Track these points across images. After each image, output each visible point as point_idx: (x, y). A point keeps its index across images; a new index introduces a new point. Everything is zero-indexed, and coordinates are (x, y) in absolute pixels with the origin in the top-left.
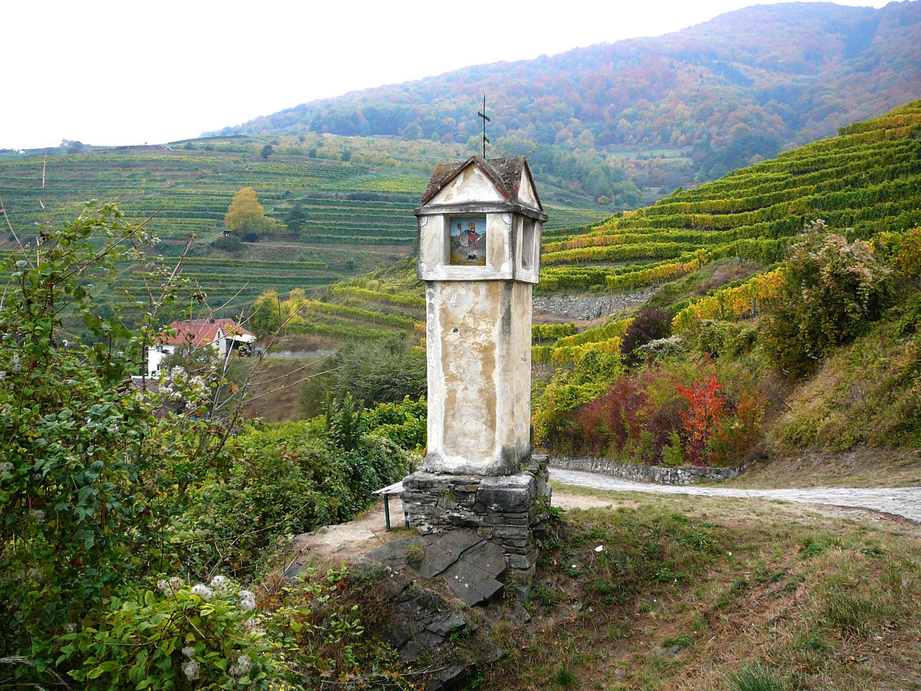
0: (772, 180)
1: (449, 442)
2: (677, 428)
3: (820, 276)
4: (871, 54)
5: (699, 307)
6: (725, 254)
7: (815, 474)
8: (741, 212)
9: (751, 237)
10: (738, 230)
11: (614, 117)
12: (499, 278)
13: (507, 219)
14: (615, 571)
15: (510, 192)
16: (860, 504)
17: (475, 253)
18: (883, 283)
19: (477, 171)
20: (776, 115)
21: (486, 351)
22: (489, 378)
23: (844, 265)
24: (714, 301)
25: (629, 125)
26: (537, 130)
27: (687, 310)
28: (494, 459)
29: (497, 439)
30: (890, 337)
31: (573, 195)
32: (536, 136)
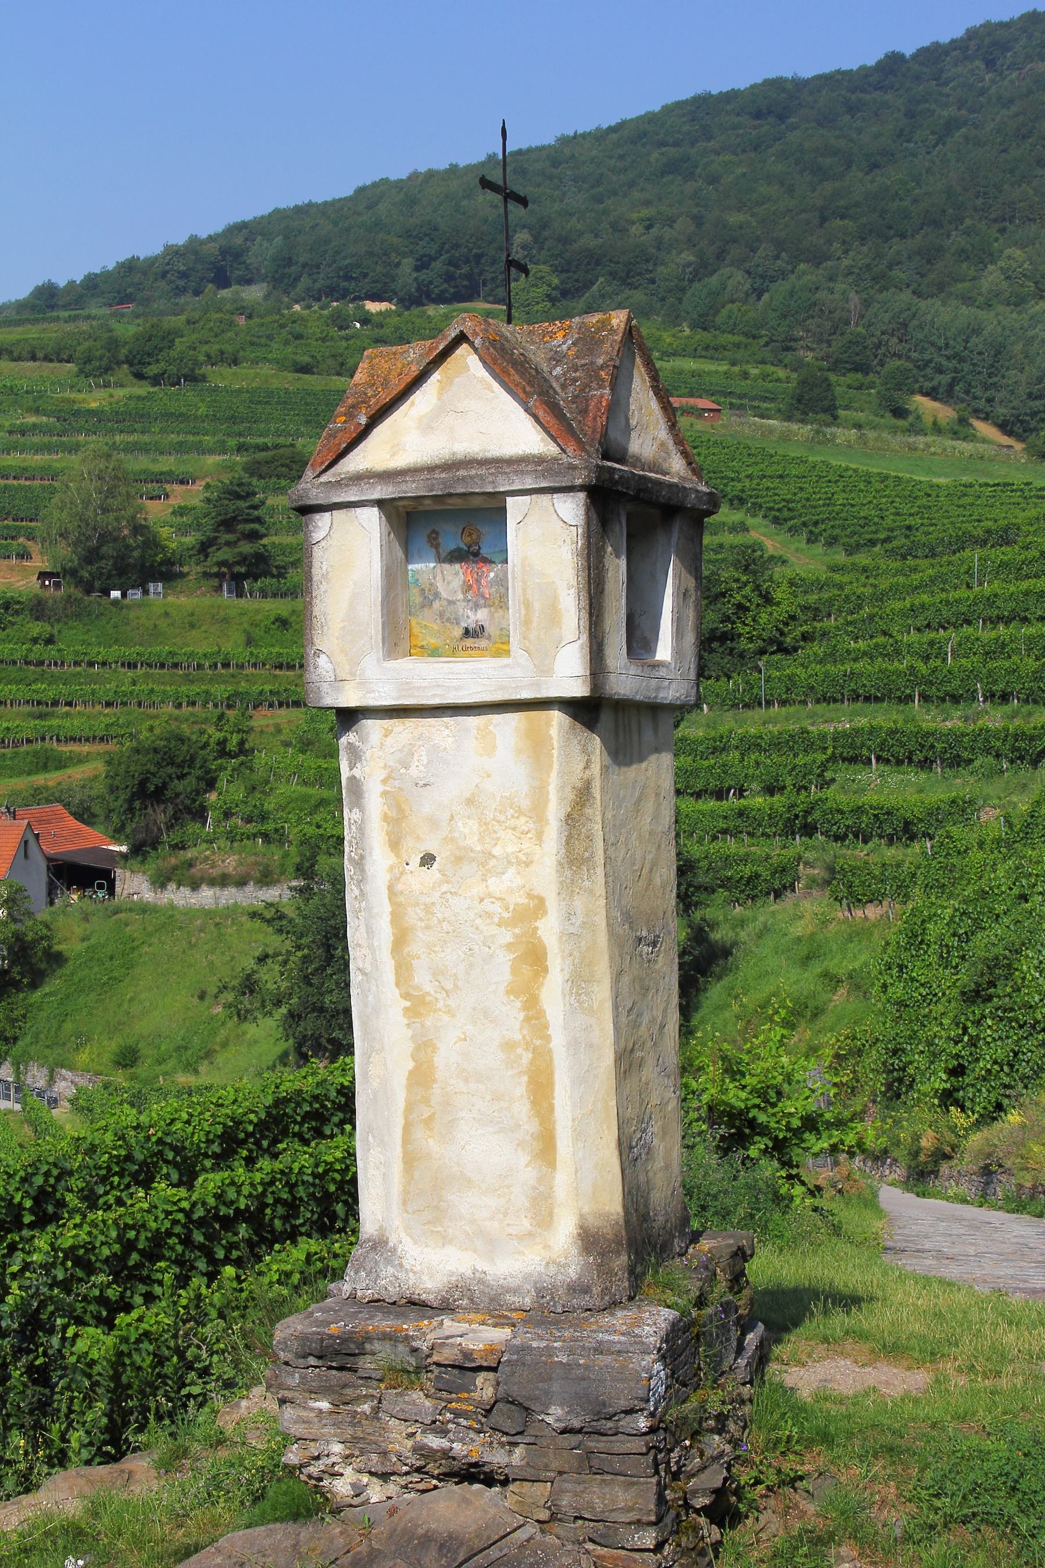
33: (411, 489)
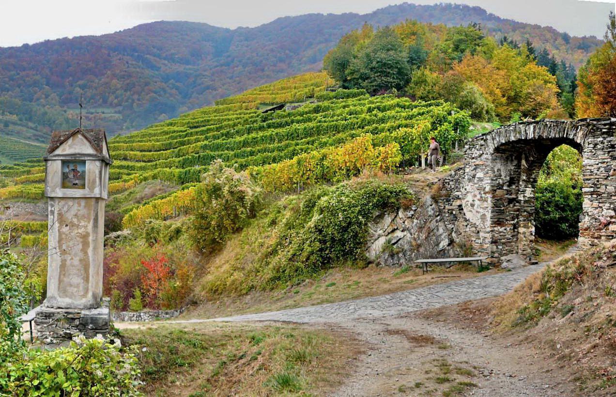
0: (178, 132)
1: (61, 289)
2: (139, 287)
4: (229, 56)
5: (140, 211)
6: (151, 178)
7: (229, 310)
8: (158, 151)
9: (166, 167)
10: (158, 162)
11: (72, 86)
12: (93, 196)
13: (98, 163)
14: (155, 362)
17: (77, 182)
18: (256, 197)
19: (80, 136)
20: (174, 90)
21: (85, 237)
22: (86, 253)
23: (236, 186)
24: (149, 207)
25: (82, 91)
26: (21, 92)
27: (132, 213)
28: (89, 299)
29: (90, 288)
30: (263, 227)
31: (45, 136)
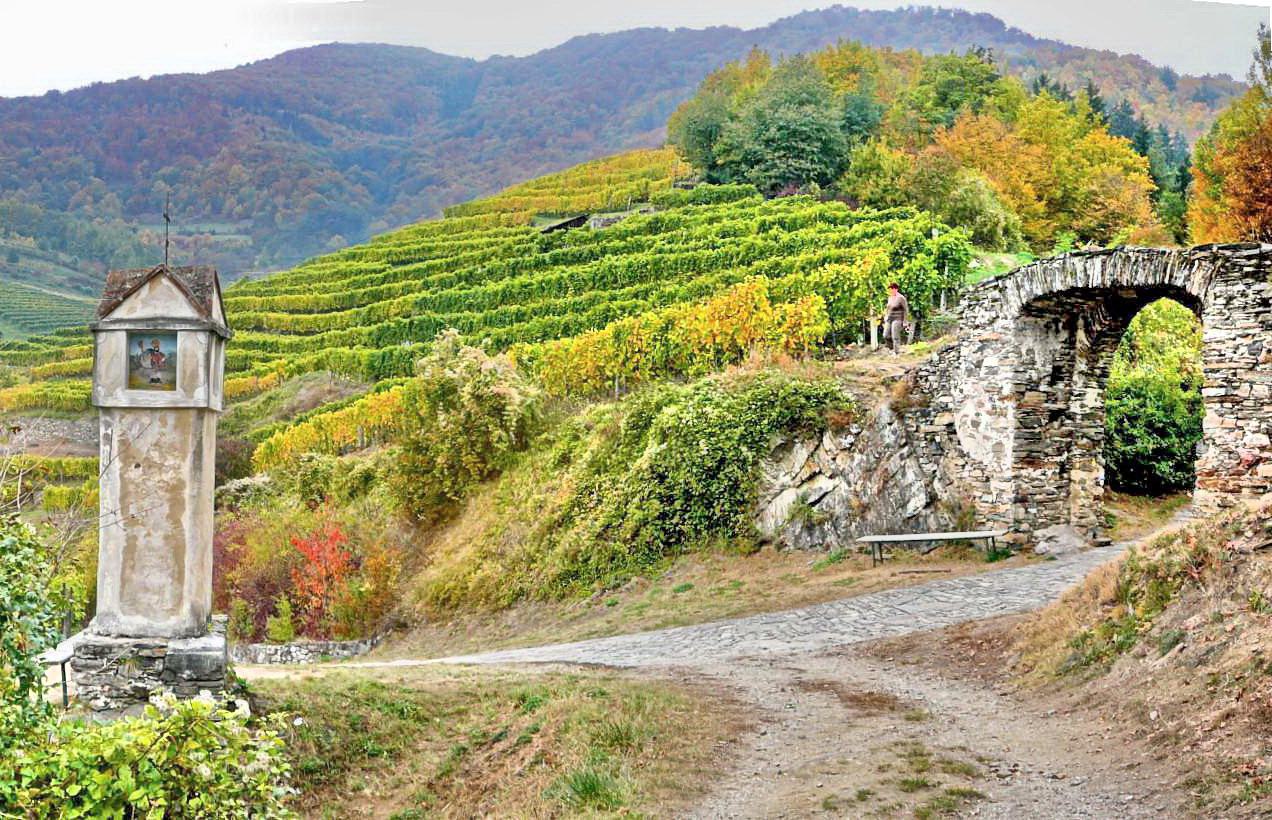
0: (367, 272)
1: (126, 598)
2: (287, 593)
3: (460, 398)
4: (473, 116)
5: (291, 437)
6: (311, 367)
7: (473, 639)
9: (343, 345)
10: (326, 335)
12: (192, 405)
13: (202, 338)
14: (320, 747)
15: (203, 307)
16: (552, 659)
18: (530, 406)
19: (165, 281)
21: (175, 489)
23: (487, 385)
24: (308, 427)
25: (168, 189)
27: (271, 440)
28: (184, 618)
29: (185, 594)
31: (92, 280)
32: (42, 199)
33: (140, 327)
